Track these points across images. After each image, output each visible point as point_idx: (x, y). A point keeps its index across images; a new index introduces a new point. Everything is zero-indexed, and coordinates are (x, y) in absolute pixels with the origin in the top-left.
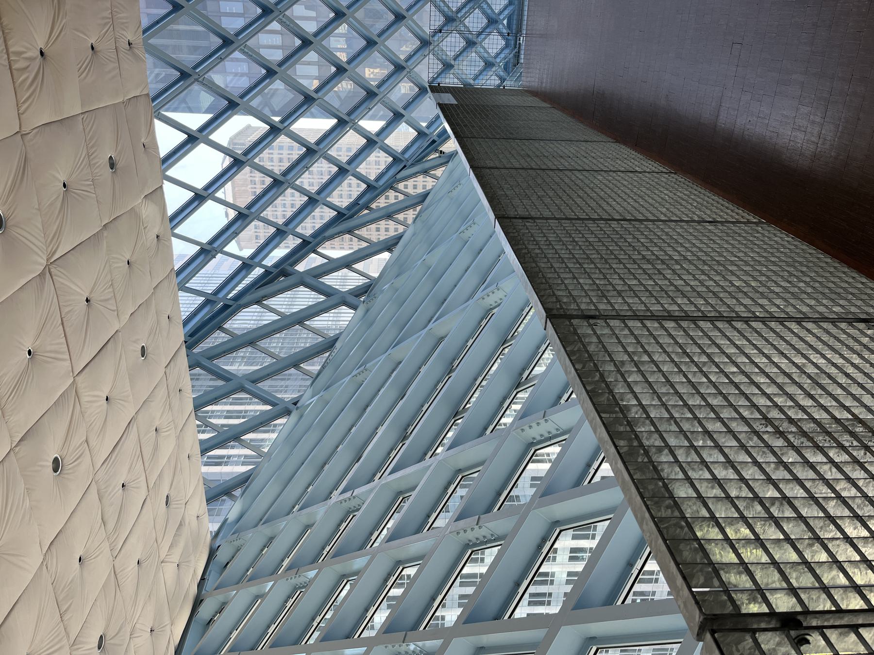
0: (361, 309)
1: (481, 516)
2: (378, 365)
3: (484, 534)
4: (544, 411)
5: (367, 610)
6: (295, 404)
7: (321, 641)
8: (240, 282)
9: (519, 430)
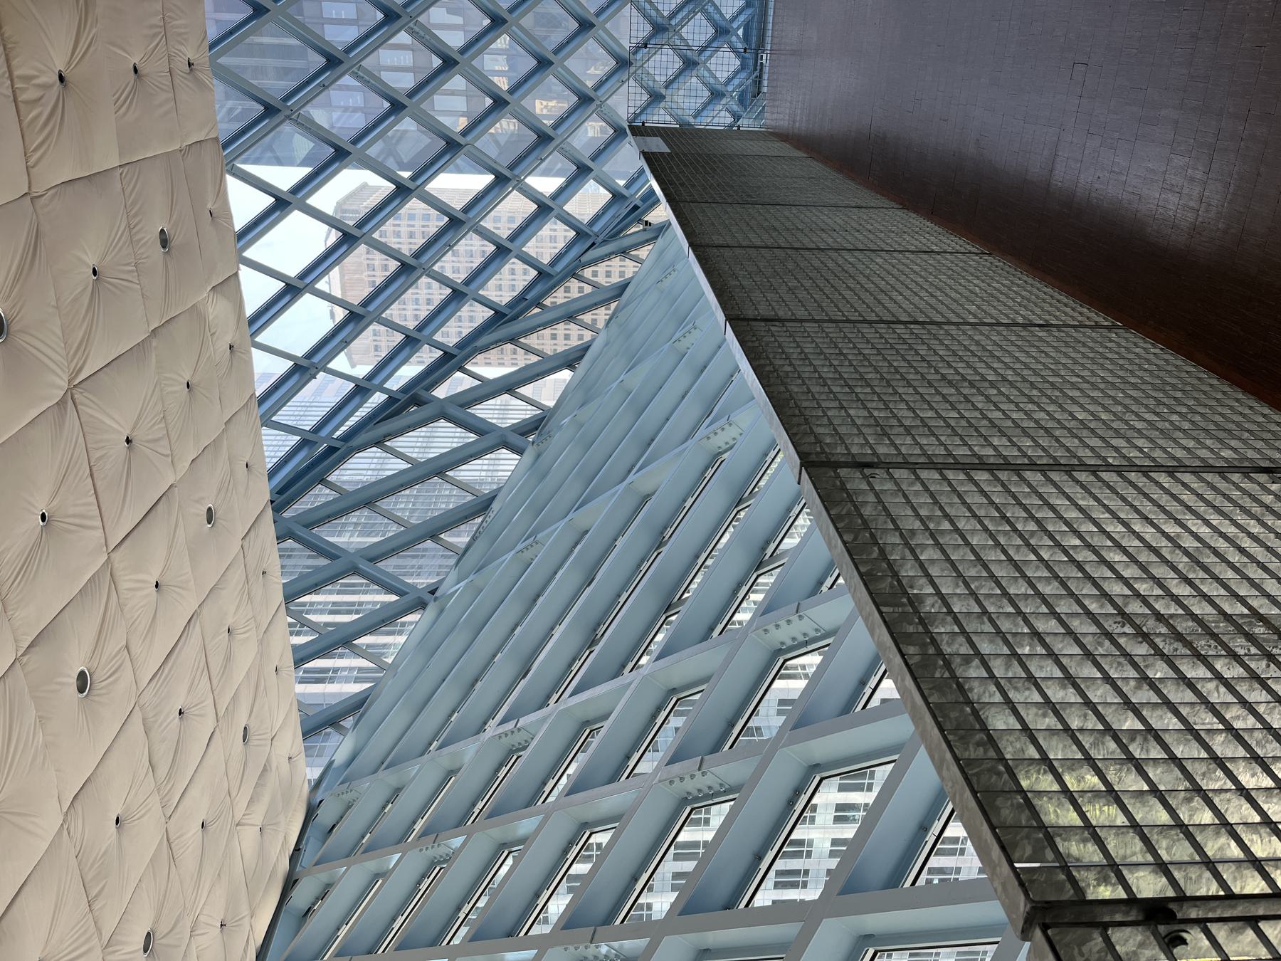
0: (530, 453)
1: (706, 757)
2: (554, 536)
3: (709, 783)
4: (797, 604)
5: (537, 895)
6: (433, 592)
7: (470, 941)
8: (351, 414)
9: (761, 632)
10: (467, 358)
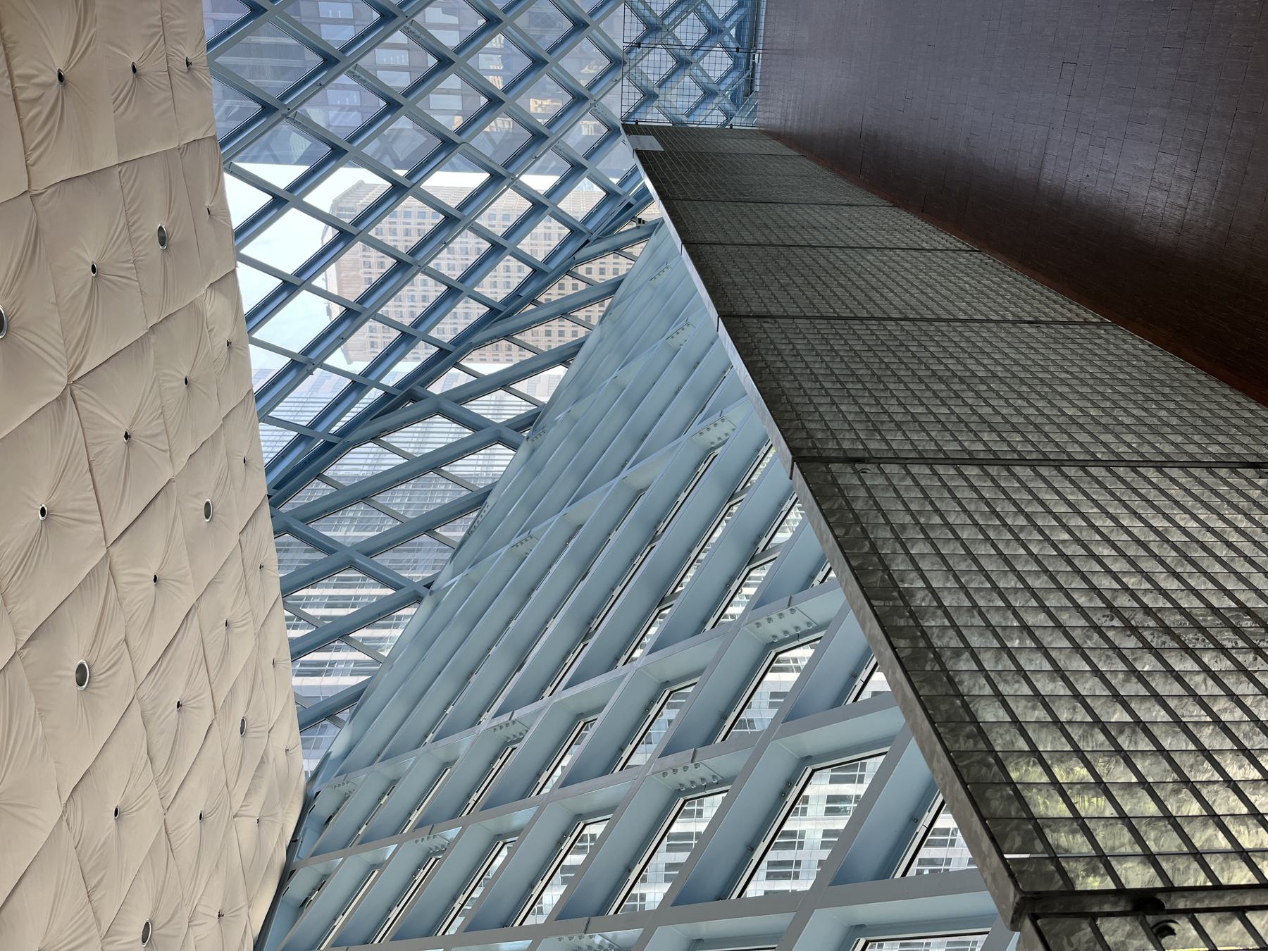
0: (524, 449)
1: (699, 750)
2: (549, 530)
3: (702, 775)
4: (789, 597)
5: (532, 886)
6: (428, 586)
7: (465, 931)
8: (348, 410)
9: (753, 625)
10: (463, 354)
